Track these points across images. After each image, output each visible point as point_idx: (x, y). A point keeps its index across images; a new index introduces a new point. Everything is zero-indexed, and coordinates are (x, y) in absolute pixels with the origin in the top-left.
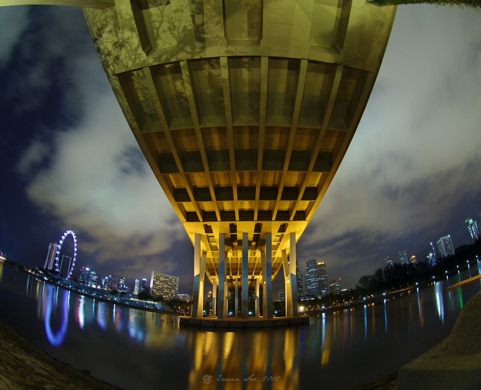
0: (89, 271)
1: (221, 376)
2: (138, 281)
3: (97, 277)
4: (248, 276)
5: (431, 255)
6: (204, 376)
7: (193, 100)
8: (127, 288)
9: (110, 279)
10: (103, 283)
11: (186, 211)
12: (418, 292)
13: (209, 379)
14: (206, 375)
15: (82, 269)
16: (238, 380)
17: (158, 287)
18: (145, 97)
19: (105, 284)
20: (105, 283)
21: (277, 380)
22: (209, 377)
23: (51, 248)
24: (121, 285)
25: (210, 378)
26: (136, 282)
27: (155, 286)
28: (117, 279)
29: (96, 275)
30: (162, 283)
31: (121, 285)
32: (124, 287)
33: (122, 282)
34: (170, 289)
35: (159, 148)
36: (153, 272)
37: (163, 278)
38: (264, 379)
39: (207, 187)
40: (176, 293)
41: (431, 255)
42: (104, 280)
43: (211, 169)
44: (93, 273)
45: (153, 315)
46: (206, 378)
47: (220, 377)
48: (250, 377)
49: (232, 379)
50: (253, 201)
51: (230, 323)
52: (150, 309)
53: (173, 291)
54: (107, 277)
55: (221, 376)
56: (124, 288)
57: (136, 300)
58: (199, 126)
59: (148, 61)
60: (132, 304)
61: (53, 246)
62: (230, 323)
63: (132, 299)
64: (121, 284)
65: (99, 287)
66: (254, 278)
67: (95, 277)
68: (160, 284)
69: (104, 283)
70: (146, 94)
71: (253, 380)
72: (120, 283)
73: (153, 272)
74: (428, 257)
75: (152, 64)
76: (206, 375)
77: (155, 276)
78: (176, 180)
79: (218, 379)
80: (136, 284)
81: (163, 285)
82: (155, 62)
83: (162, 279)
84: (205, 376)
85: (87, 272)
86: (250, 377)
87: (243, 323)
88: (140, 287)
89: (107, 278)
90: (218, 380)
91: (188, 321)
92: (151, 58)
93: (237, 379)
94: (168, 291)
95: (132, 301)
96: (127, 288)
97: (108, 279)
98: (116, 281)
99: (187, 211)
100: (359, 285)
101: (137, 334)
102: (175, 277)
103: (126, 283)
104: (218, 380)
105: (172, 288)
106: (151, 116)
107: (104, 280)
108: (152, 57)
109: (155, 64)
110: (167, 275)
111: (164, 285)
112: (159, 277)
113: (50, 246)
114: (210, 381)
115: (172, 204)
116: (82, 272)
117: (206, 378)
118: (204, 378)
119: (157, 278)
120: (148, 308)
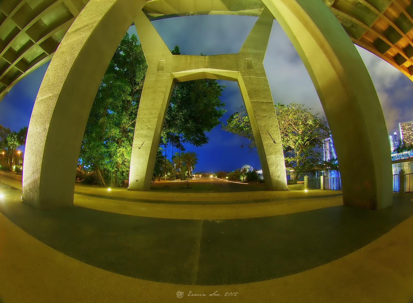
1: (191, 292)
4: (76, 187)
7: (367, 3)
11: (406, 67)
14: (179, 291)
16: (205, 295)
18: (341, 20)
21: (235, 295)
22: (181, 293)
25: (182, 294)
27: (404, 136)
35: (370, 40)
39: (408, 44)
43: (405, 33)
45: (409, 164)
46: (179, 293)
47: (190, 293)
49: (200, 295)
50: (390, 49)
55: (191, 292)
58: (381, 14)
59: (328, 5)
68: (407, 133)
70: (340, 18)
71: (217, 295)
73: (399, 124)
75: (331, 4)
76: (179, 291)
78: (392, 52)
79: (188, 294)
81: (409, 133)
82: (332, 2)
83: (407, 127)
84: (178, 292)
88: (393, 141)
90: (189, 295)
92: (328, 2)
99: (407, 67)
104: (189, 295)
106: (353, 26)
108: (327, 1)
109: (333, 3)
115: (397, 68)
117: (179, 293)
119: (403, 128)
120: (405, 159)
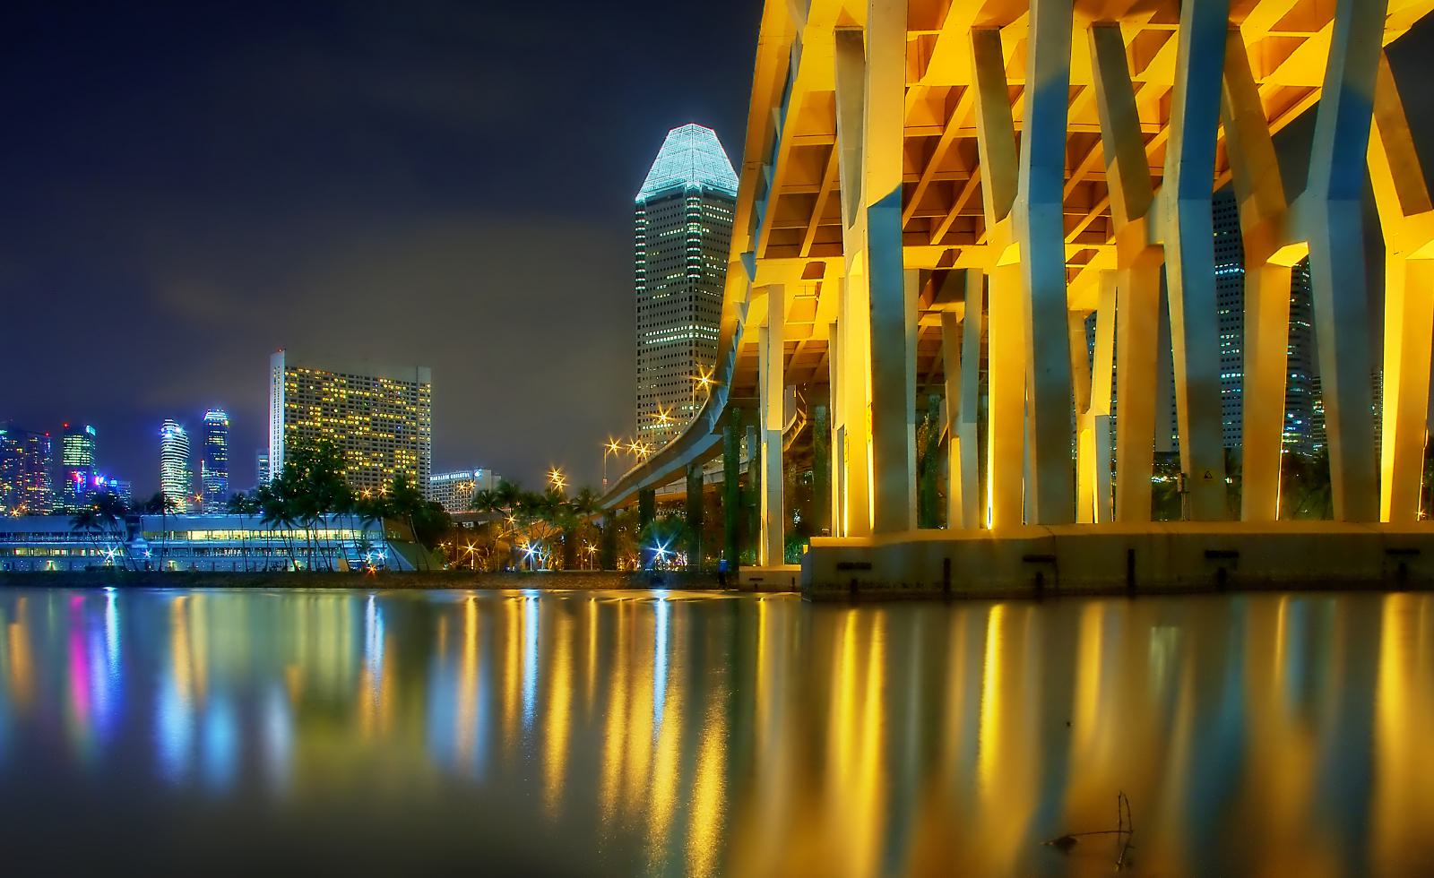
2: (179, 430)
8: (114, 483)
17: (318, 445)
24: (78, 474)
32: (99, 481)
34: (389, 447)
36: (279, 360)
37: (343, 386)
40: (420, 466)
51: (1131, 555)
52: (345, 573)
56: (96, 488)
57: (221, 535)
60: (202, 565)
62: (1131, 555)
63: (198, 536)
66: (958, 265)
68: (325, 425)
72: (67, 462)
77: (294, 380)
80: (167, 449)
88: (193, 464)
91: (866, 567)
95: (201, 550)
96: (114, 483)
98: (42, 456)
101: (627, 735)
105: (400, 441)
112: (319, 385)
119: (302, 399)
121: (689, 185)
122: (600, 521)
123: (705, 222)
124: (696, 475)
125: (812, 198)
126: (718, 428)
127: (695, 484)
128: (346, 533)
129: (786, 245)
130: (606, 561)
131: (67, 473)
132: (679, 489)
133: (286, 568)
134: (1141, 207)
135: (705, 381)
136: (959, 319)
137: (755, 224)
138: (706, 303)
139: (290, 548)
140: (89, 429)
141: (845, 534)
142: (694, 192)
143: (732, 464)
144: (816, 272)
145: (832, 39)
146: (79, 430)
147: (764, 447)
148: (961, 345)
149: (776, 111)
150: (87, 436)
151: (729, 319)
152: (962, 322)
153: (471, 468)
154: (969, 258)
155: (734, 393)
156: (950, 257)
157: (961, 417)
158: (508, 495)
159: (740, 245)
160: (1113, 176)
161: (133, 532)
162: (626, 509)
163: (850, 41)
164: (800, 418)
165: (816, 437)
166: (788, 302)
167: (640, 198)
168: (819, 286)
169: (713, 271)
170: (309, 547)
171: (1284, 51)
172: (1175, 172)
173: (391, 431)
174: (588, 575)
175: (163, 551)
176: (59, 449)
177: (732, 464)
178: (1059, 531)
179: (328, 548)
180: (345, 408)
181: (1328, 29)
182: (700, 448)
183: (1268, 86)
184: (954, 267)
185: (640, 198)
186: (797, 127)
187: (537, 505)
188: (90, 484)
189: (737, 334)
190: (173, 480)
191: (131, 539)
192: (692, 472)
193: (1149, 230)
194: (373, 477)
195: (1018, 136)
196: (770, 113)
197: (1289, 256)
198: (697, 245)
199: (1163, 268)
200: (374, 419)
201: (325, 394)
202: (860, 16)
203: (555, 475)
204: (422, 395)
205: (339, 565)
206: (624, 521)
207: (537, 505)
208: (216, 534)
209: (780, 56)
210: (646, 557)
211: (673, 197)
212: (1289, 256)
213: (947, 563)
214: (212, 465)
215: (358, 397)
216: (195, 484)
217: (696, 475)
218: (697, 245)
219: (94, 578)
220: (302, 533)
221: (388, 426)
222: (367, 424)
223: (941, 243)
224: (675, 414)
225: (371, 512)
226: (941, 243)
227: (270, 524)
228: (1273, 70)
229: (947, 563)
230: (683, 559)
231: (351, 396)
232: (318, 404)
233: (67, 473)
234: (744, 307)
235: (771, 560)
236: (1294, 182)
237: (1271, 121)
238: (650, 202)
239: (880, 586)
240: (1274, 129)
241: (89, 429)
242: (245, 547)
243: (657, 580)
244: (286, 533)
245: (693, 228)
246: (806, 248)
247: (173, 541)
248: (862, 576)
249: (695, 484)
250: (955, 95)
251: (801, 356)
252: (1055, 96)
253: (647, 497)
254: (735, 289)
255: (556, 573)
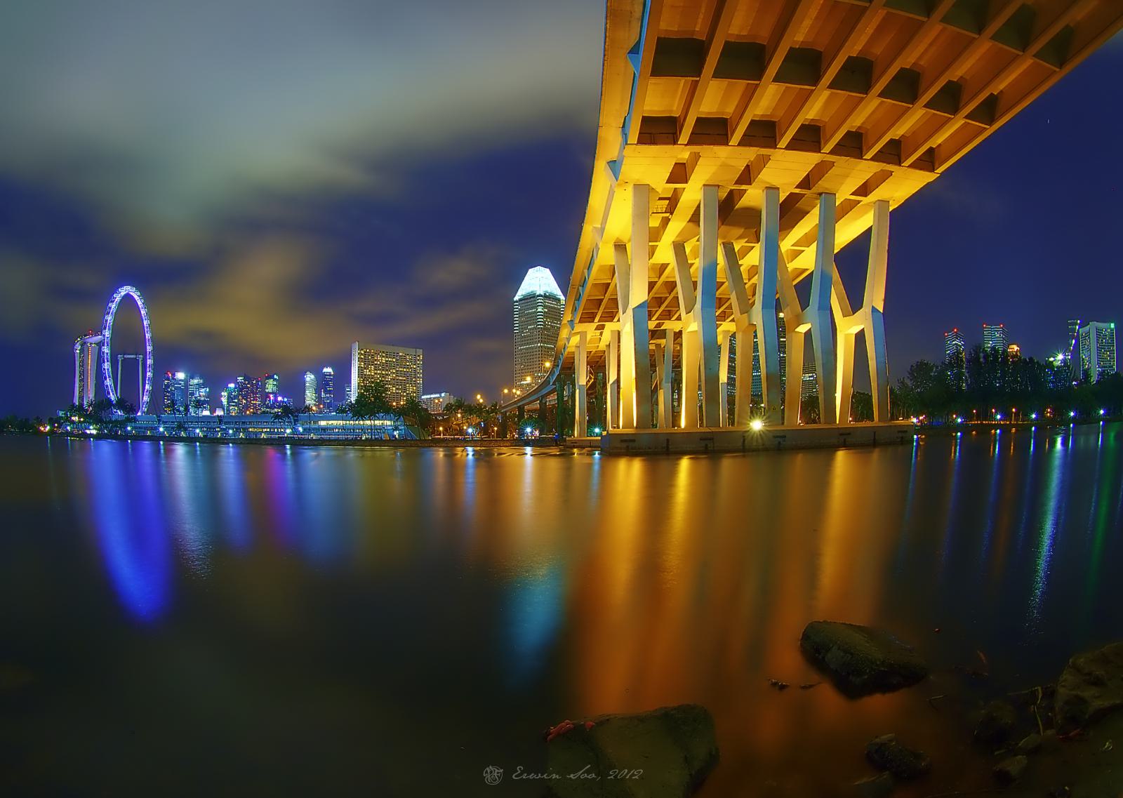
0: (186, 381)
1: (520, 769)
3: (208, 390)
5: (1060, 357)
6: (486, 768)
8: (286, 400)
9: (241, 388)
10: (224, 401)
12: (1031, 453)
13: (496, 774)
15: (168, 379)
19: (228, 403)
20: (230, 399)
22: (497, 771)
23: (82, 351)
24: (271, 396)
25: (498, 773)
26: (308, 379)
28: (258, 381)
29: (204, 385)
30: (380, 370)
31: (271, 396)
32: (280, 399)
33: (271, 386)
37: (383, 357)
38: (611, 775)
41: (1060, 357)
42: (226, 394)
44: (196, 381)
46: (491, 772)
47: (519, 772)
48: (581, 772)
49: (545, 776)
53: (411, 389)
54: (230, 383)
61: (85, 343)
63: (323, 423)
64: (271, 393)
65: (219, 412)
67: (203, 393)
68: (375, 374)
69: (228, 399)
71: (589, 777)
72: (267, 391)
74: (1052, 359)
76: (491, 767)
84: (487, 769)
85: (180, 384)
86: (581, 772)
87: (622, 441)
88: (317, 391)
89: (232, 386)
90: (516, 776)
91: (634, 441)
93: (554, 775)
94: (397, 389)
95: (324, 429)
97: (236, 388)
100: (909, 383)
102: (412, 351)
103: (282, 390)
104: (516, 776)
107: (226, 394)
110: (391, 349)
111: (387, 375)
113: (78, 347)
114: (499, 778)
116: (168, 386)
118: (487, 772)
119: (366, 361)
121: (538, 294)
122: (499, 416)
123: (545, 307)
124: (544, 402)
125: (602, 300)
126: (554, 384)
127: (543, 404)
128: (389, 423)
129: (588, 317)
130: (502, 434)
131: (267, 395)
132: (537, 405)
133: (361, 438)
134: (746, 307)
135: (548, 364)
136: (662, 346)
137: (575, 310)
138: (552, 335)
139: (363, 429)
140: (275, 377)
141: (621, 427)
142: (540, 296)
143: (560, 397)
144: (600, 328)
145: (612, 249)
146: (272, 377)
147: (577, 391)
148: (664, 355)
149: (586, 271)
150: (275, 380)
151: (560, 343)
152: (664, 347)
153: (440, 393)
154: (671, 326)
155: (563, 369)
156: (659, 325)
157: (664, 380)
158: (459, 405)
159: (567, 317)
160: (733, 297)
161: (296, 421)
162: (511, 412)
163: (620, 247)
164: (590, 378)
165: (598, 387)
166: (589, 337)
167: (516, 298)
168: (601, 334)
169: (548, 325)
170: (372, 428)
171: (796, 254)
172: (760, 299)
173: (404, 377)
174: (496, 440)
175: (307, 431)
176: (264, 387)
177: (560, 397)
178: (714, 429)
179: (382, 428)
180: (386, 366)
181: (814, 246)
182: (544, 391)
183: (791, 266)
184: (661, 328)
185: (516, 298)
186: (595, 276)
187: (471, 410)
188: (276, 400)
189: (564, 348)
190: (310, 398)
191: (295, 424)
192: (542, 400)
193: (749, 317)
194: (397, 397)
195: (695, 283)
196: (583, 271)
197: (803, 329)
198: (542, 315)
199: (755, 332)
200: (398, 371)
201: (376, 360)
202: (625, 238)
203: (479, 397)
204: (418, 360)
205: (385, 437)
206: (510, 417)
207: (471, 410)
208: (330, 422)
209: (588, 252)
210: (522, 433)
211: (531, 298)
212: (803, 329)
213: (668, 440)
214: (326, 392)
215: (401, 371)
216: (319, 400)
217: (544, 402)
218: (542, 315)
219: (280, 442)
220: (368, 422)
221: (405, 374)
222: (394, 373)
223: (657, 319)
224: (534, 378)
225: (400, 413)
226: (657, 319)
227: (355, 418)
228: (792, 261)
229: (668, 440)
230: (537, 433)
231: (386, 361)
232: (372, 365)
233: (267, 395)
234: (568, 340)
235: (580, 435)
236: (804, 303)
237: (793, 280)
238: (520, 300)
239: (639, 449)
240: (795, 283)
241: (275, 377)
242: (343, 428)
243: (527, 443)
244: (361, 422)
245: (540, 309)
246: (597, 319)
247: (313, 426)
248: (631, 444)
249: (543, 404)
250: (663, 267)
251: (592, 356)
252: (710, 271)
253: (521, 409)
254: (564, 333)
255: (482, 440)
